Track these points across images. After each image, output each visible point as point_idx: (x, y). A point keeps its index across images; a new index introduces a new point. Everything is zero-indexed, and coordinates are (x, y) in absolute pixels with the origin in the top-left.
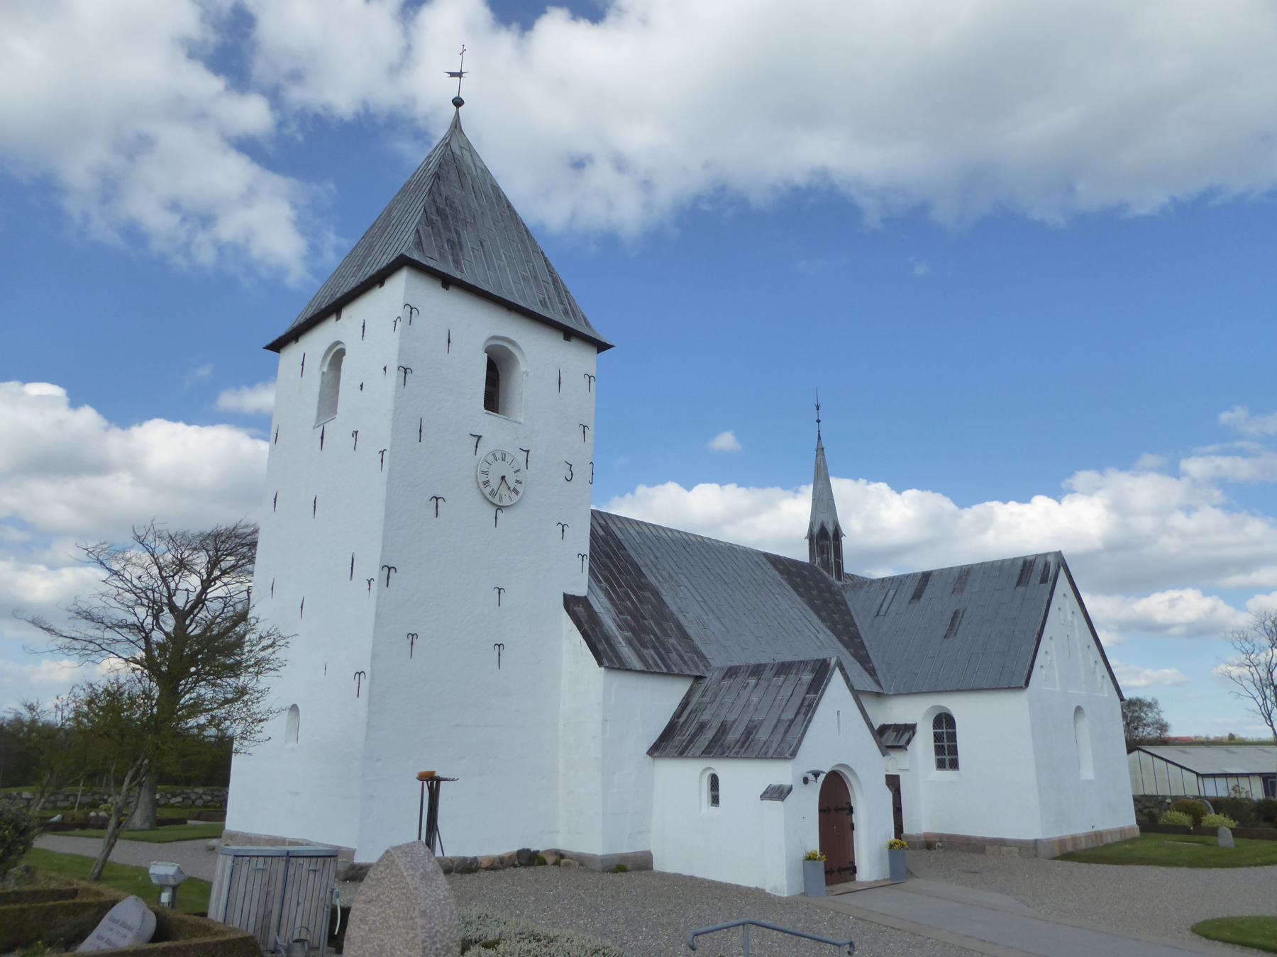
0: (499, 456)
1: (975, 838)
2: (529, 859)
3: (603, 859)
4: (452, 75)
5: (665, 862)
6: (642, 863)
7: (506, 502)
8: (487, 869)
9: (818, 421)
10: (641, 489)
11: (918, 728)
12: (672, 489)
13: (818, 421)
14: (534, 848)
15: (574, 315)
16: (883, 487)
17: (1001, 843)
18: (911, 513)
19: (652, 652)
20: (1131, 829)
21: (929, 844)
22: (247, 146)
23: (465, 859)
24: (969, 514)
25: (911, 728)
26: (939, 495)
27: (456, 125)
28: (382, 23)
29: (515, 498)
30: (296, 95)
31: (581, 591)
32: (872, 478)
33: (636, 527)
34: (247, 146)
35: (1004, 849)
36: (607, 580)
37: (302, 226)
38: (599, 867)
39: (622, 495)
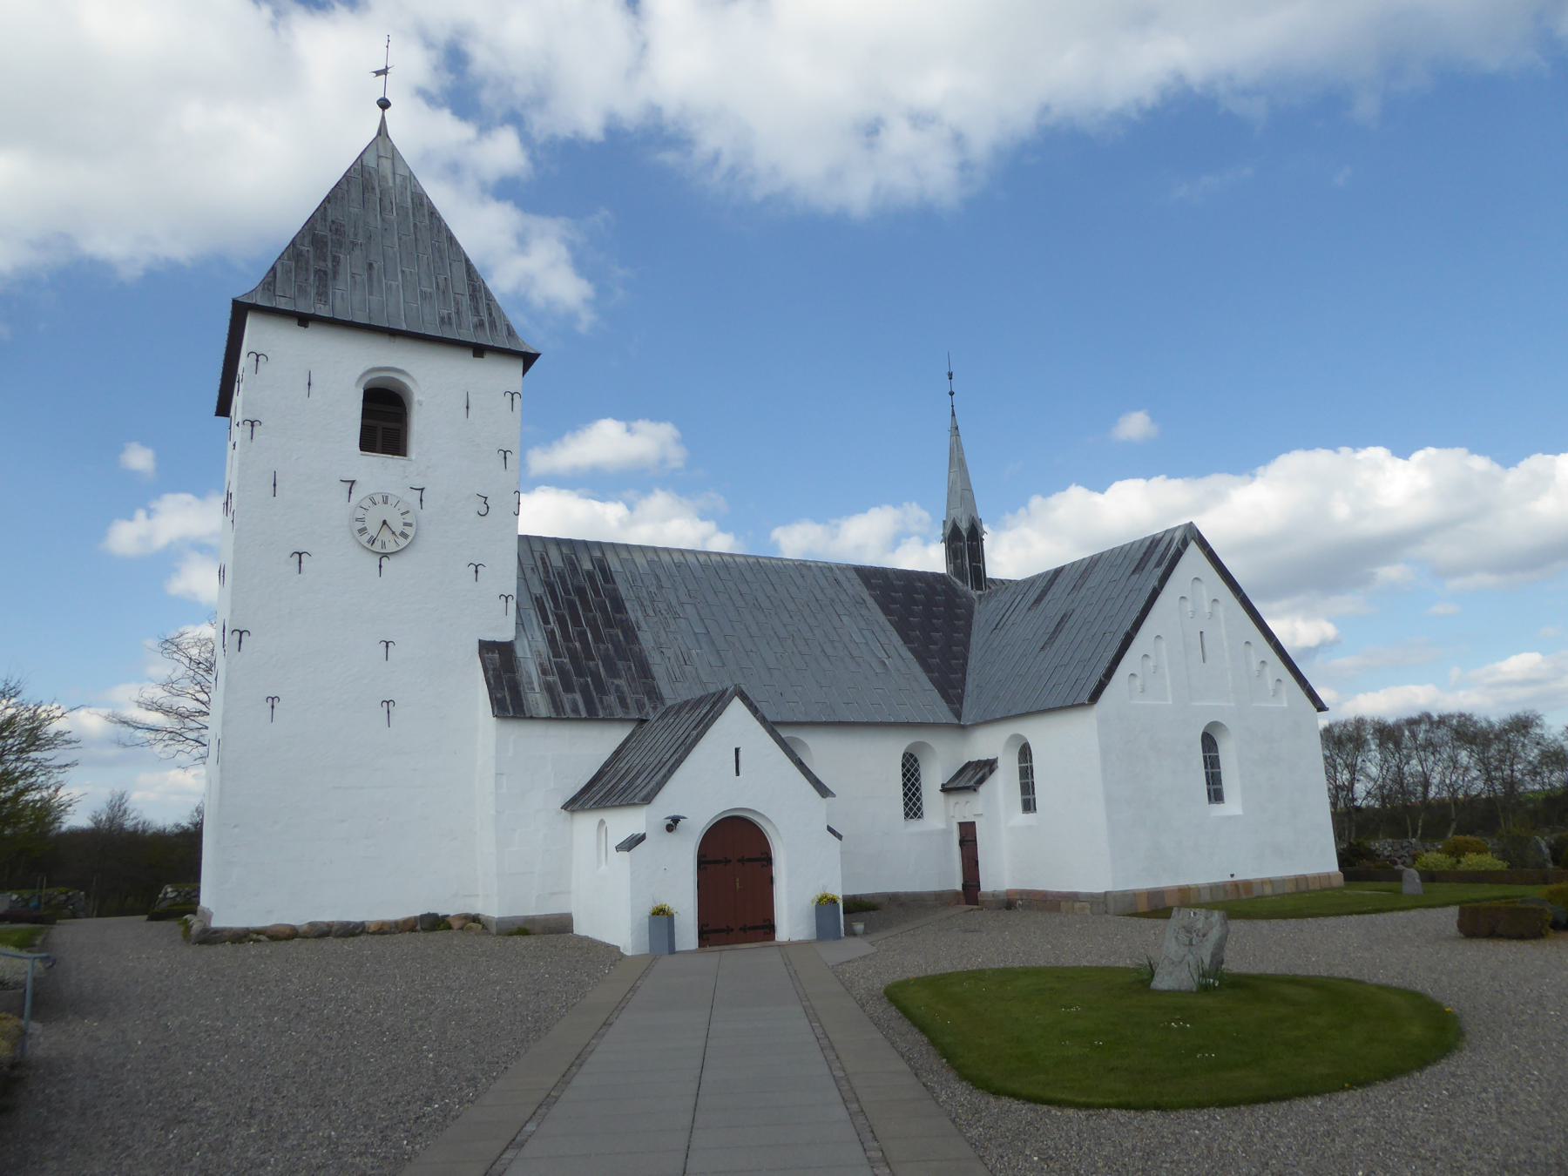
0: (378, 499)
1: (906, 894)
2: (434, 923)
3: (501, 921)
4: (378, 73)
5: (581, 928)
6: (560, 926)
7: (391, 548)
8: (373, 933)
9: (952, 394)
10: (1036, 501)
11: (1000, 763)
12: (1076, 496)
13: (952, 394)
14: (441, 912)
15: (493, 325)
16: (1378, 453)
17: (1073, 897)
18: (1423, 480)
19: (578, 697)
20: (1328, 876)
21: (1008, 903)
22: (505, 190)
23: (349, 923)
24: (1514, 477)
25: (989, 766)
26: (1460, 452)
27: (382, 131)
28: (612, 18)
29: (403, 542)
30: (540, 123)
31: (506, 633)
32: (1358, 443)
33: (624, 555)
34: (505, 190)
35: (1077, 905)
36: (561, 621)
37: (581, 265)
38: (494, 930)
39: (1014, 512)
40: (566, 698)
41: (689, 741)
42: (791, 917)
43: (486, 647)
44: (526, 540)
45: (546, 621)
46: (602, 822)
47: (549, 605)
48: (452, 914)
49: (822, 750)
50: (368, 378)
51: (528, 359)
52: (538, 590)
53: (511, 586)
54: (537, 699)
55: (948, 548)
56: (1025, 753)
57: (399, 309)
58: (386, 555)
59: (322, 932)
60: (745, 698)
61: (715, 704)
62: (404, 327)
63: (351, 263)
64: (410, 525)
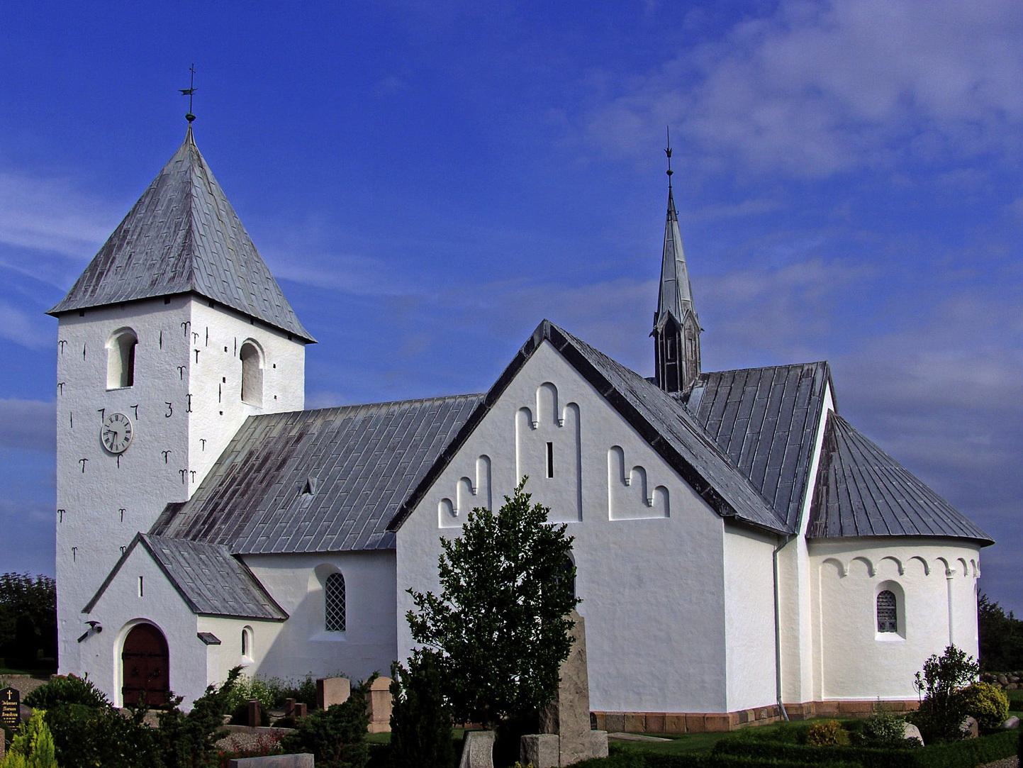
9: (670, 173)
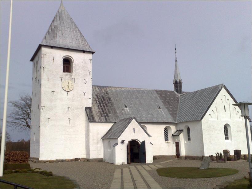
8: (67, 162)
9: (176, 53)
13: (176, 53)
31: (90, 105)
40: (102, 118)
41: (123, 130)
42: (149, 159)
43: (86, 108)
44: (128, 163)
45: (97, 103)
46: (109, 141)
47: (97, 99)
48: (81, 158)
49: (149, 127)
50: (64, 57)
51: (93, 53)
52: (95, 97)
53: (91, 97)
54: (97, 119)
55: (174, 85)
56: (188, 129)
57: (69, 43)
58: (68, 91)
59: (57, 161)
60: (135, 119)
61: (130, 120)
62: (70, 48)
63: (59, 34)
64: (72, 86)
